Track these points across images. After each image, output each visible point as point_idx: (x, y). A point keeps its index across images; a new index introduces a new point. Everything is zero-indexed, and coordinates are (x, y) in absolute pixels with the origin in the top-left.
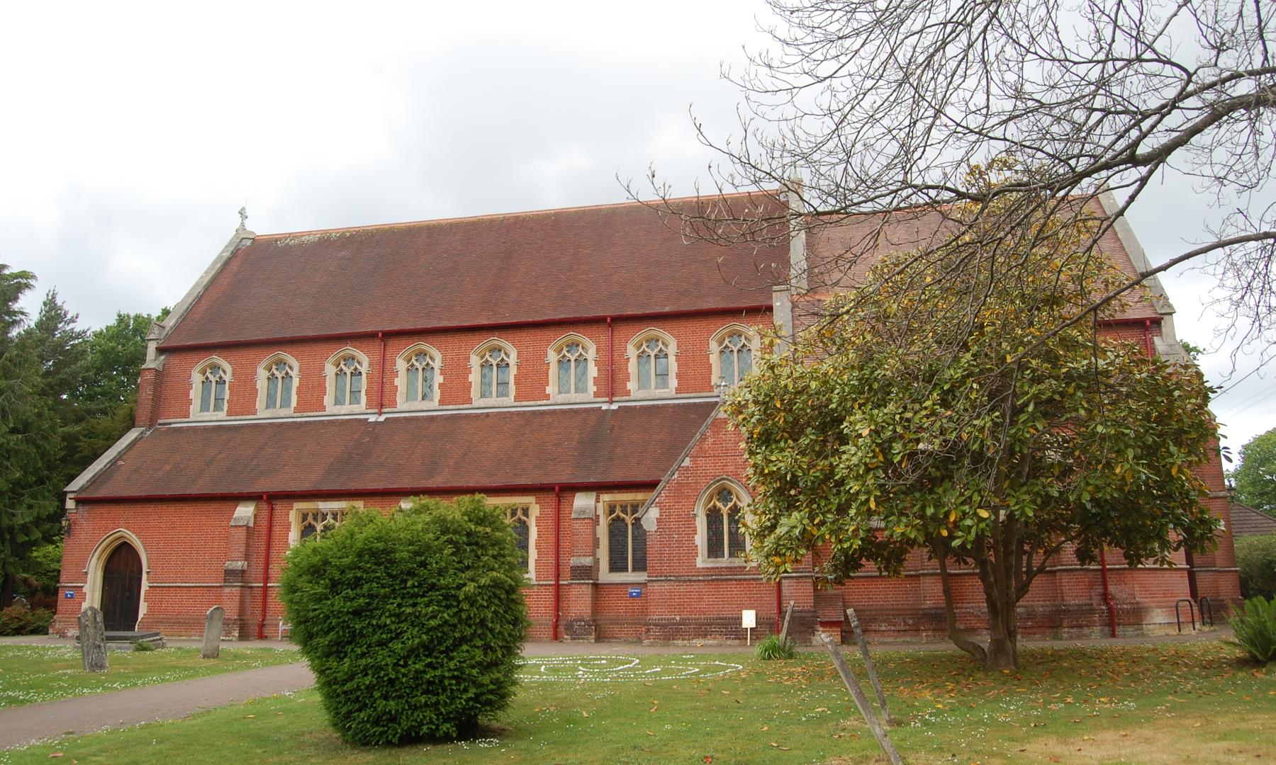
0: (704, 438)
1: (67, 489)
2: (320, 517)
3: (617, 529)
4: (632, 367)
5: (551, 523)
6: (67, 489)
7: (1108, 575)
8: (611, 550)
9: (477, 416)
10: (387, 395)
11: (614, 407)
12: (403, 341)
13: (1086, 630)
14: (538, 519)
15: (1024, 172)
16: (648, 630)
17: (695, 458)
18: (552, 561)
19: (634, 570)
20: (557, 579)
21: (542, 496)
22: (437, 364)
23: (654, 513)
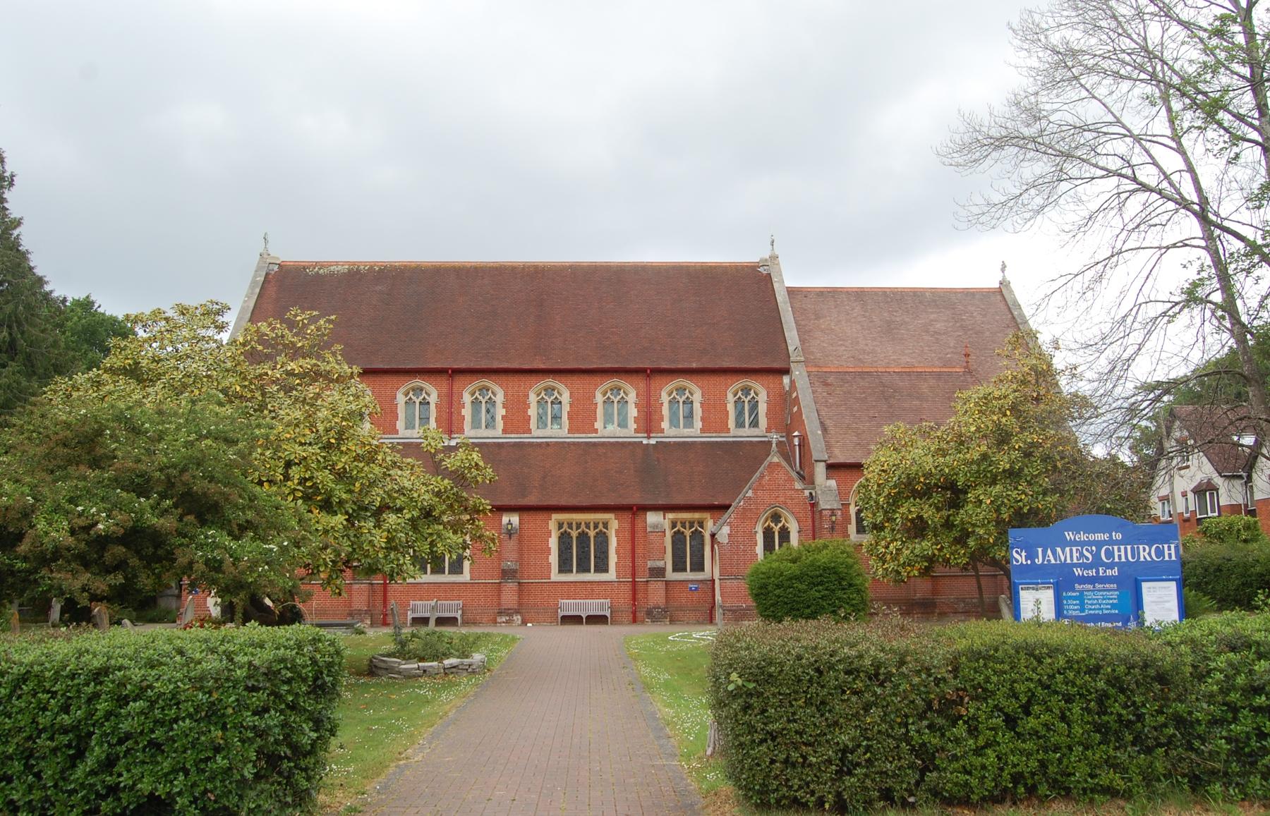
0: (762, 476)
3: (678, 539)
4: (665, 411)
8: (607, 557)
9: (540, 445)
11: (653, 441)
12: (468, 378)
17: (755, 491)
19: (432, 572)
20: (634, 575)
21: (620, 513)
23: (726, 530)
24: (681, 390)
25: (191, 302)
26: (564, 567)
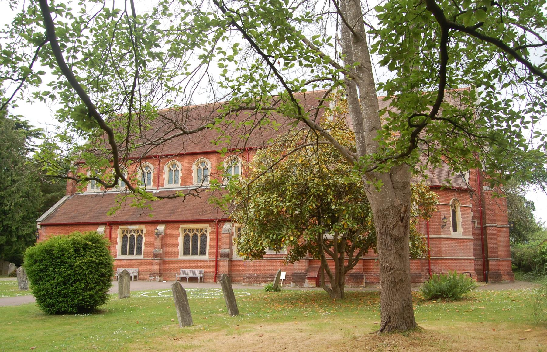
1: (37, 220)
2: (129, 232)
5: (215, 235)
6: (37, 220)
7: (431, 261)
10: (161, 182)
13: (417, 284)
14: (210, 233)
15: (391, 93)
16: (244, 279)
18: (215, 250)
19: (200, 254)
22: (180, 169)
24: (203, 163)
25: (535, 205)
26: (124, 252)
